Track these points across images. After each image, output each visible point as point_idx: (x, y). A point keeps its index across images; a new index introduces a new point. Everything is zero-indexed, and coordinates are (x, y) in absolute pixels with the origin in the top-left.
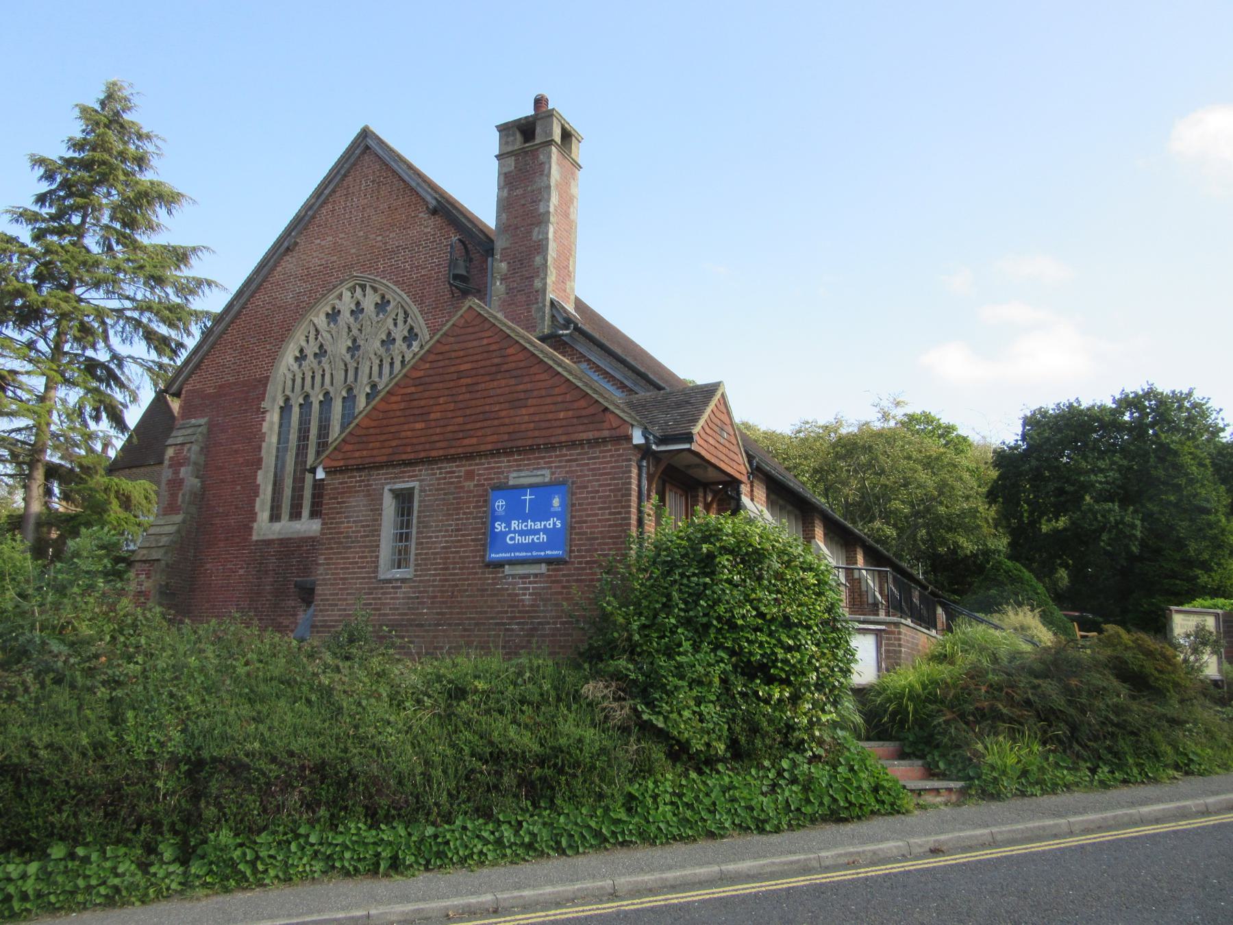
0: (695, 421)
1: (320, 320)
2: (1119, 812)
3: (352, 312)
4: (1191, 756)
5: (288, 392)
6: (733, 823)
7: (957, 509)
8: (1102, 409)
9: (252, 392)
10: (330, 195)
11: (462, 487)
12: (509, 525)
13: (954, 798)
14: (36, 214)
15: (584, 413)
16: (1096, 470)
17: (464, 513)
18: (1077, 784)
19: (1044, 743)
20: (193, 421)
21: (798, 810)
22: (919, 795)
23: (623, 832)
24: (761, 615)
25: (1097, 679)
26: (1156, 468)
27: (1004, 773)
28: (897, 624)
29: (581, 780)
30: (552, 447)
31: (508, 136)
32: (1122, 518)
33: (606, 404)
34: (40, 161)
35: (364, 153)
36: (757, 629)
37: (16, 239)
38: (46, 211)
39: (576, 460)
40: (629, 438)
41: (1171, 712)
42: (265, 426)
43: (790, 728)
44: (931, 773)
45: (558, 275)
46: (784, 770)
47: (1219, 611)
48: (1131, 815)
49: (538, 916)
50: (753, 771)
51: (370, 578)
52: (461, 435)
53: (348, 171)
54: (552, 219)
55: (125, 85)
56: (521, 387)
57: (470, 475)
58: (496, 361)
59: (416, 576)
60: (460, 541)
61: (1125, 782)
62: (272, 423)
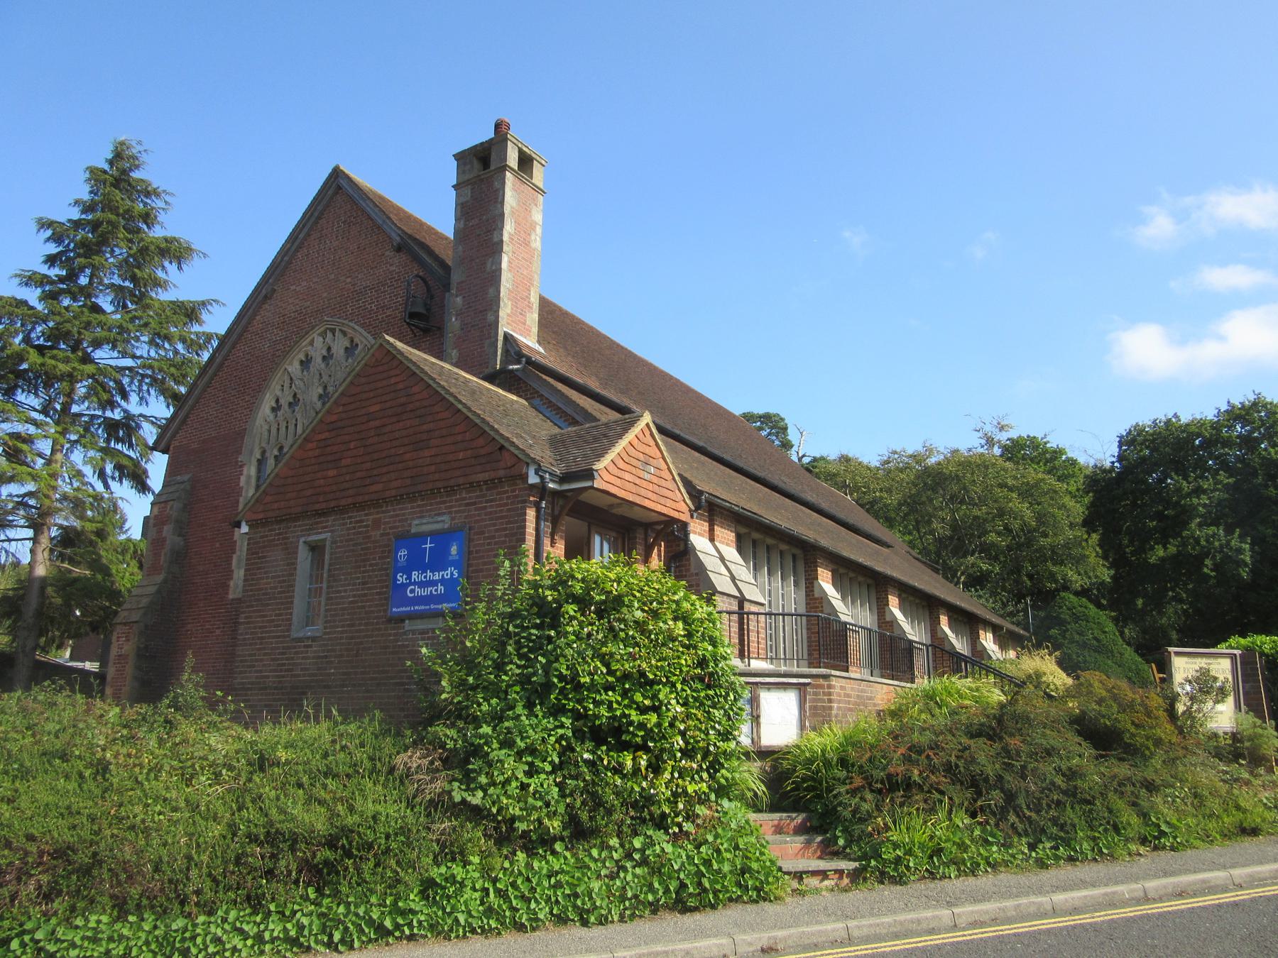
0: (600, 456)
1: (294, 367)
2: (1024, 901)
3: (324, 358)
4: (1164, 827)
5: (264, 445)
6: (551, 913)
7: (1061, 540)
8: (1201, 424)
9: (234, 440)
10: (305, 239)
11: (369, 537)
12: (409, 577)
13: (846, 881)
14: (46, 276)
15: (483, 451)
16: (1198, 491)
17: (371, 565)
18: (1006, 863)
19: (973, 815)
20: (179, 478)
21: (636, 896)
22: (801, 879)
23: (410, 925)
24: (611, 672)
25: (1052, 739)
26: (1266, 486)
27: (909, 852)
28: (826, 677)
29: (371, 864)
30: (451, 490)
31: (465, 164)
32: (1228, 543)
33: (502, 441)
34: (44, 224)
35: (336, 193)
36: (608, 687)
37: (25, 303)
38: (55, 272)
39: (475, 503)
40: (525, 477)
41: (1149, 774)
42: (243, 479)
43: (649, 800)
44: (828, 850)
45: (515, 306)
46: (635, 850)
47: (1235, 652)
48: (1040, 904)
49: (863, 949)
50: (595, 852)
51: (284, 637)
52: (368, 481)
53: (322, 213)
54: (505, 248)
55: (134, 143)
56: (425, 427)
57: (377, 524)
58: (403, 400)
59: (325, 633)
60: (365, 595)
61: (1071, 859)
62: (249, 477)
